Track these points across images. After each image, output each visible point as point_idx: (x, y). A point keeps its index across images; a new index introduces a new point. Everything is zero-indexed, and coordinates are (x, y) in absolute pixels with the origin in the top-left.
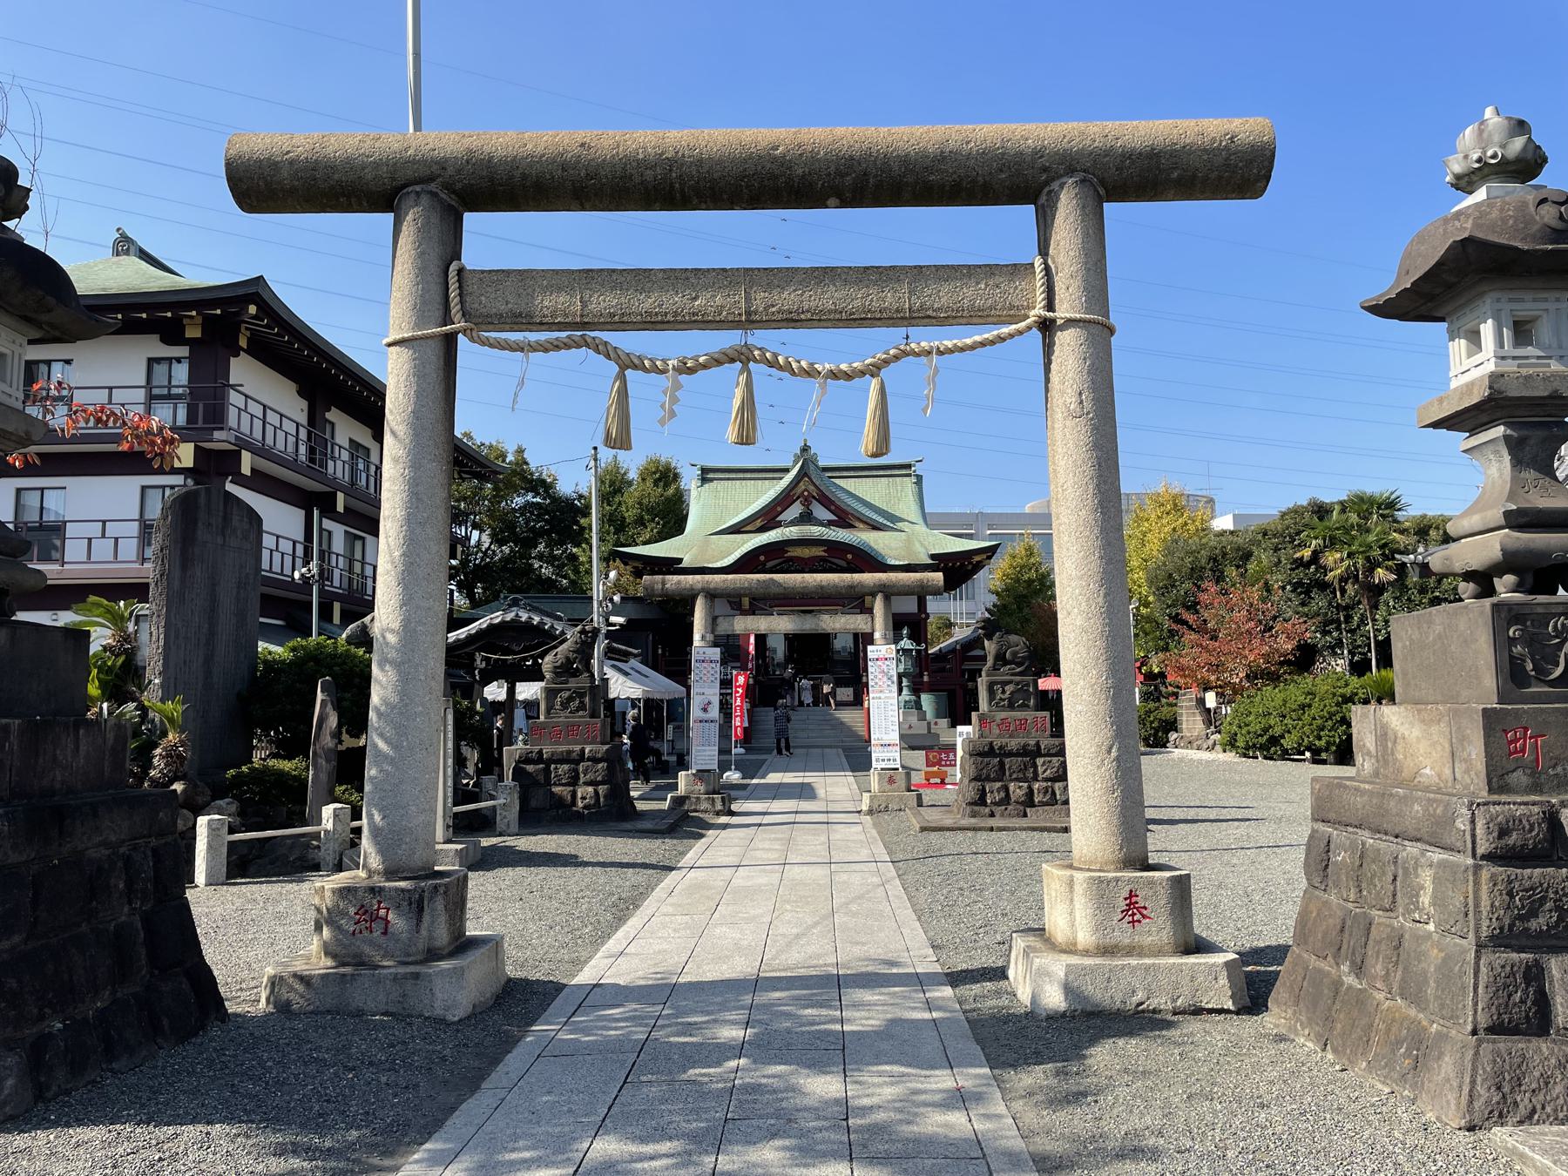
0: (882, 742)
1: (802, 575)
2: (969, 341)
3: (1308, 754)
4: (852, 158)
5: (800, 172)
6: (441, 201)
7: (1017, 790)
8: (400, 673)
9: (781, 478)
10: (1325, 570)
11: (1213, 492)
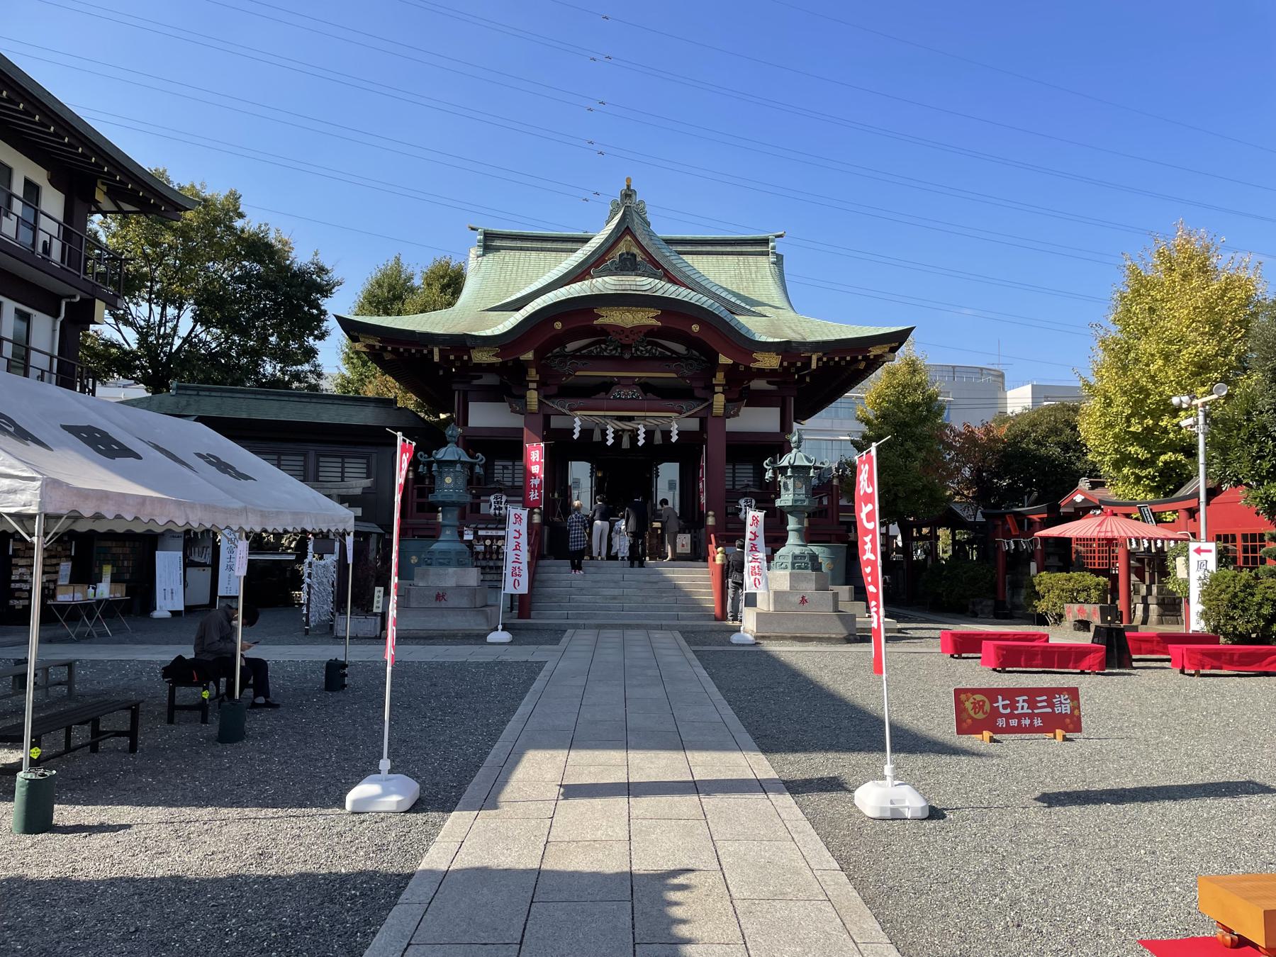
11: (1004, 367)
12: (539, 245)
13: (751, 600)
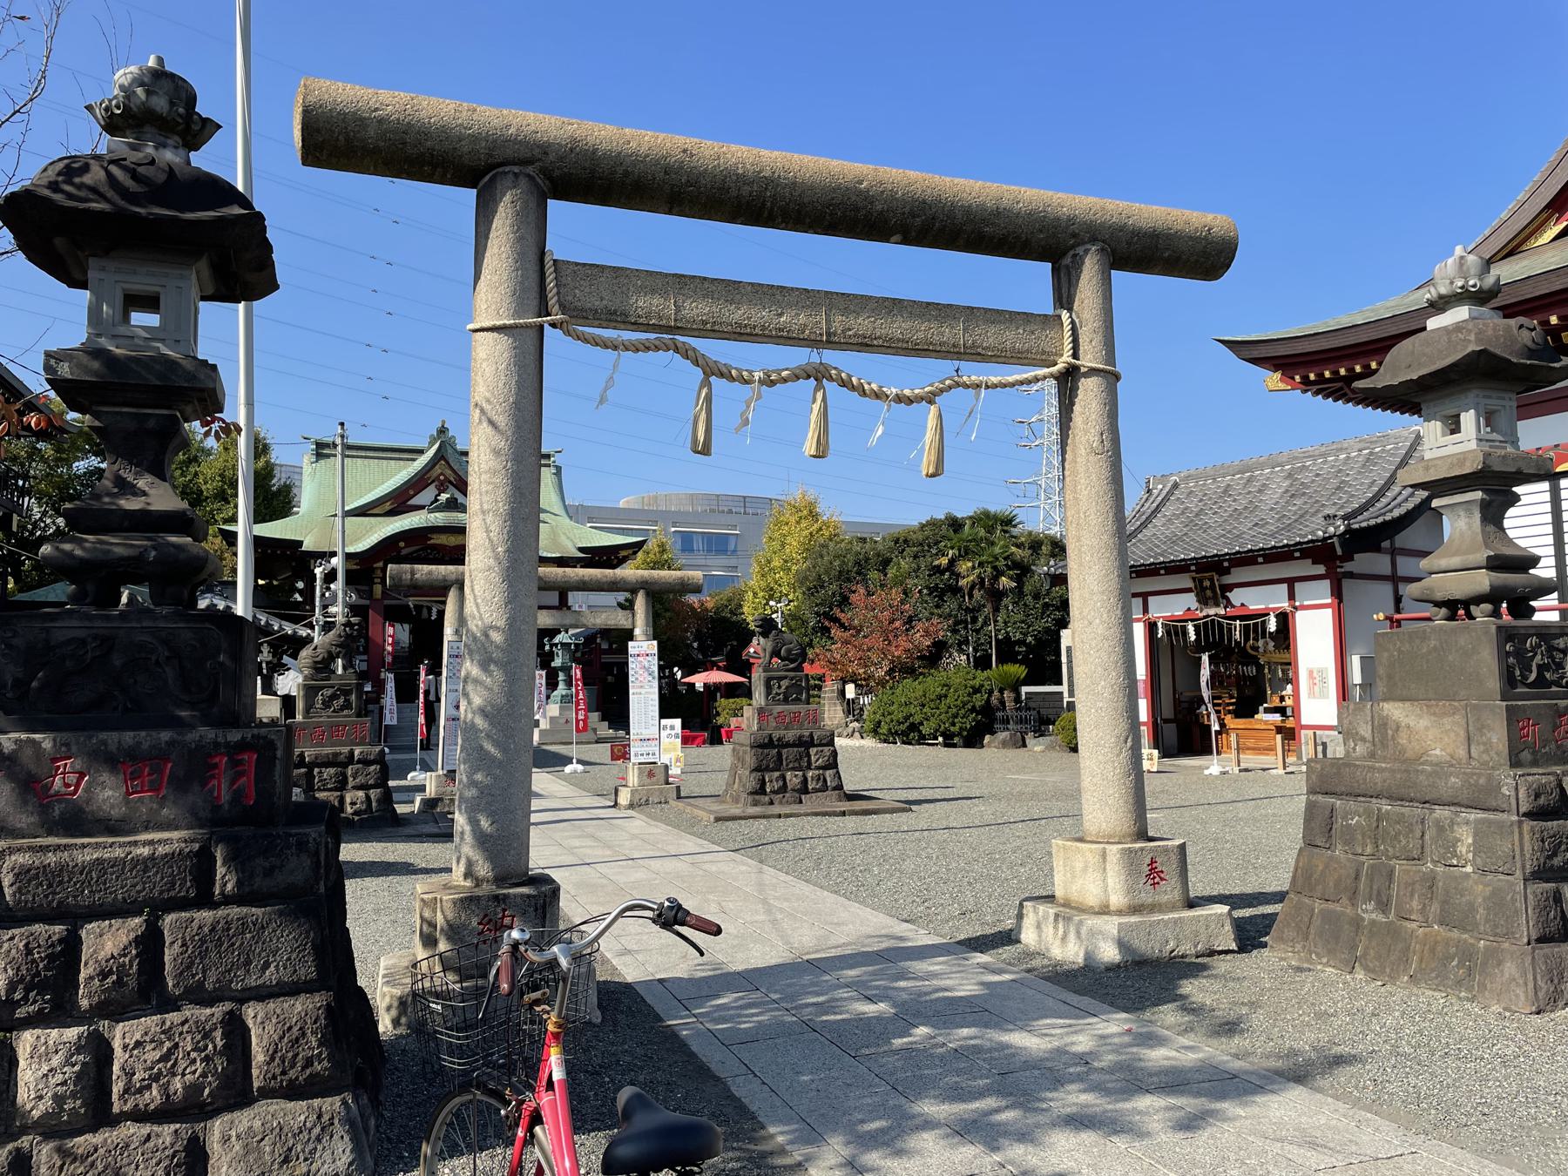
0: (642, 737)
1: (563, 569)
2: (1011, 379)
3: (940, 739)
4: (924, 202)
5: (879, 207)
6: (537, 185)
7: (793, 778)
8: (506, 673)
9: (414, 460)
10: (958, 575)
12: (363, 453)
13: (537, 724)
